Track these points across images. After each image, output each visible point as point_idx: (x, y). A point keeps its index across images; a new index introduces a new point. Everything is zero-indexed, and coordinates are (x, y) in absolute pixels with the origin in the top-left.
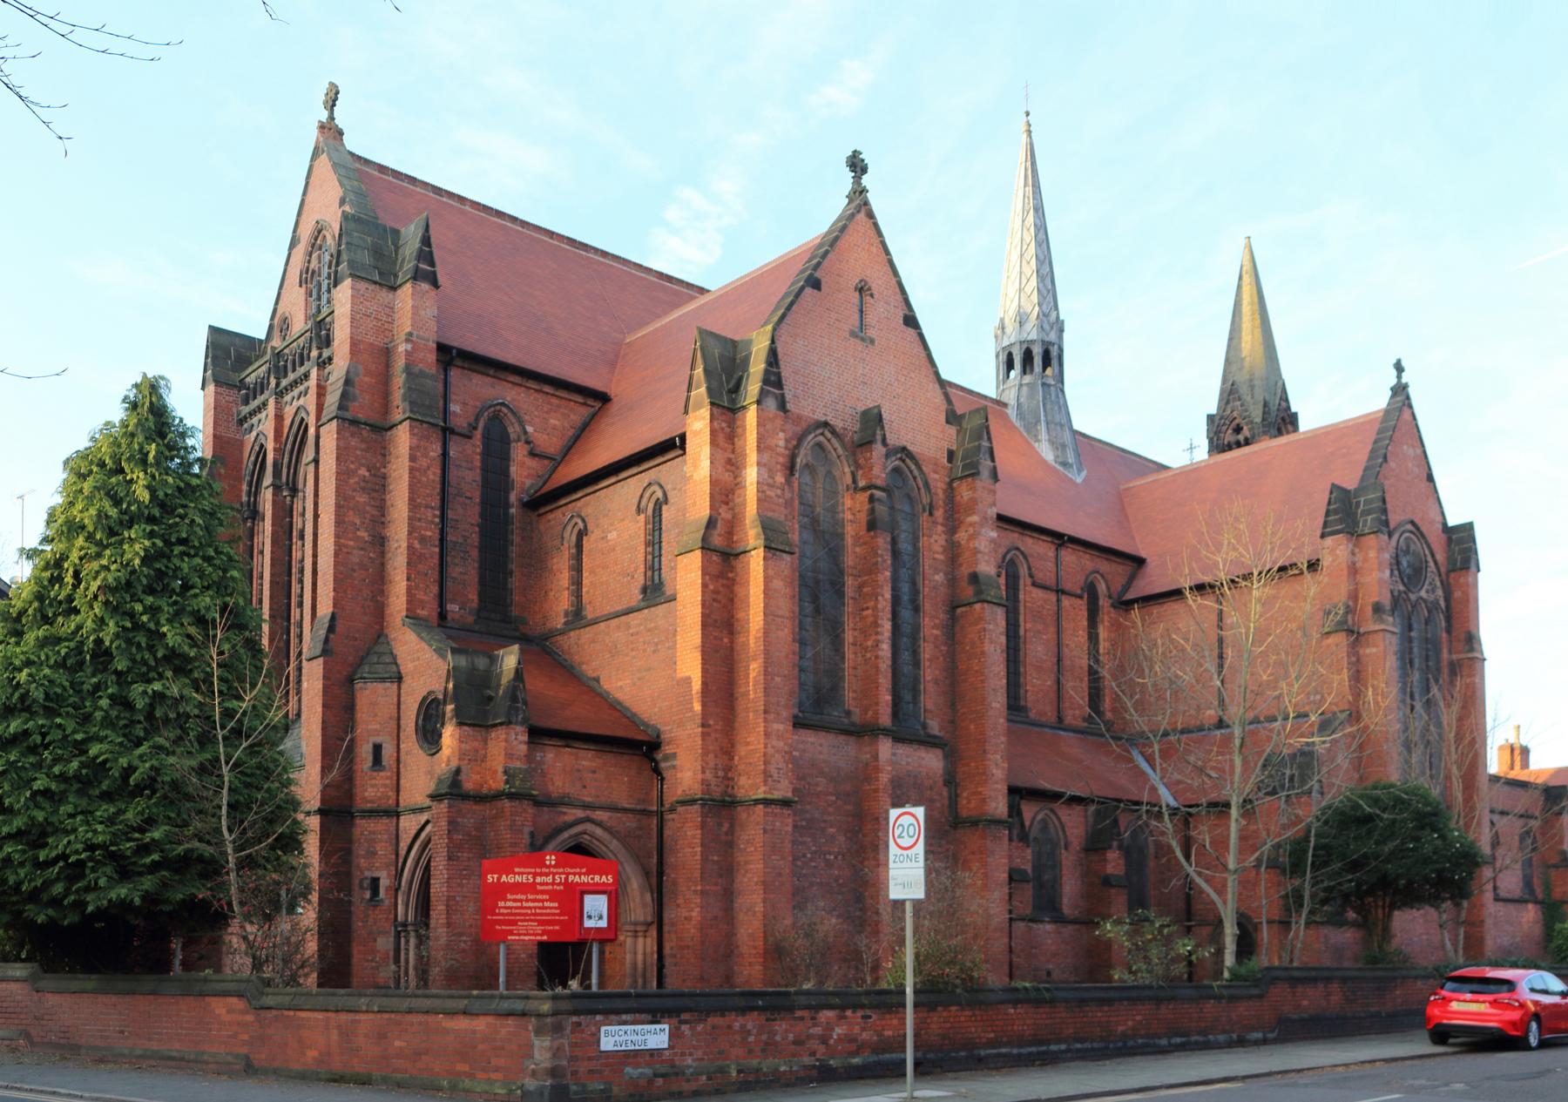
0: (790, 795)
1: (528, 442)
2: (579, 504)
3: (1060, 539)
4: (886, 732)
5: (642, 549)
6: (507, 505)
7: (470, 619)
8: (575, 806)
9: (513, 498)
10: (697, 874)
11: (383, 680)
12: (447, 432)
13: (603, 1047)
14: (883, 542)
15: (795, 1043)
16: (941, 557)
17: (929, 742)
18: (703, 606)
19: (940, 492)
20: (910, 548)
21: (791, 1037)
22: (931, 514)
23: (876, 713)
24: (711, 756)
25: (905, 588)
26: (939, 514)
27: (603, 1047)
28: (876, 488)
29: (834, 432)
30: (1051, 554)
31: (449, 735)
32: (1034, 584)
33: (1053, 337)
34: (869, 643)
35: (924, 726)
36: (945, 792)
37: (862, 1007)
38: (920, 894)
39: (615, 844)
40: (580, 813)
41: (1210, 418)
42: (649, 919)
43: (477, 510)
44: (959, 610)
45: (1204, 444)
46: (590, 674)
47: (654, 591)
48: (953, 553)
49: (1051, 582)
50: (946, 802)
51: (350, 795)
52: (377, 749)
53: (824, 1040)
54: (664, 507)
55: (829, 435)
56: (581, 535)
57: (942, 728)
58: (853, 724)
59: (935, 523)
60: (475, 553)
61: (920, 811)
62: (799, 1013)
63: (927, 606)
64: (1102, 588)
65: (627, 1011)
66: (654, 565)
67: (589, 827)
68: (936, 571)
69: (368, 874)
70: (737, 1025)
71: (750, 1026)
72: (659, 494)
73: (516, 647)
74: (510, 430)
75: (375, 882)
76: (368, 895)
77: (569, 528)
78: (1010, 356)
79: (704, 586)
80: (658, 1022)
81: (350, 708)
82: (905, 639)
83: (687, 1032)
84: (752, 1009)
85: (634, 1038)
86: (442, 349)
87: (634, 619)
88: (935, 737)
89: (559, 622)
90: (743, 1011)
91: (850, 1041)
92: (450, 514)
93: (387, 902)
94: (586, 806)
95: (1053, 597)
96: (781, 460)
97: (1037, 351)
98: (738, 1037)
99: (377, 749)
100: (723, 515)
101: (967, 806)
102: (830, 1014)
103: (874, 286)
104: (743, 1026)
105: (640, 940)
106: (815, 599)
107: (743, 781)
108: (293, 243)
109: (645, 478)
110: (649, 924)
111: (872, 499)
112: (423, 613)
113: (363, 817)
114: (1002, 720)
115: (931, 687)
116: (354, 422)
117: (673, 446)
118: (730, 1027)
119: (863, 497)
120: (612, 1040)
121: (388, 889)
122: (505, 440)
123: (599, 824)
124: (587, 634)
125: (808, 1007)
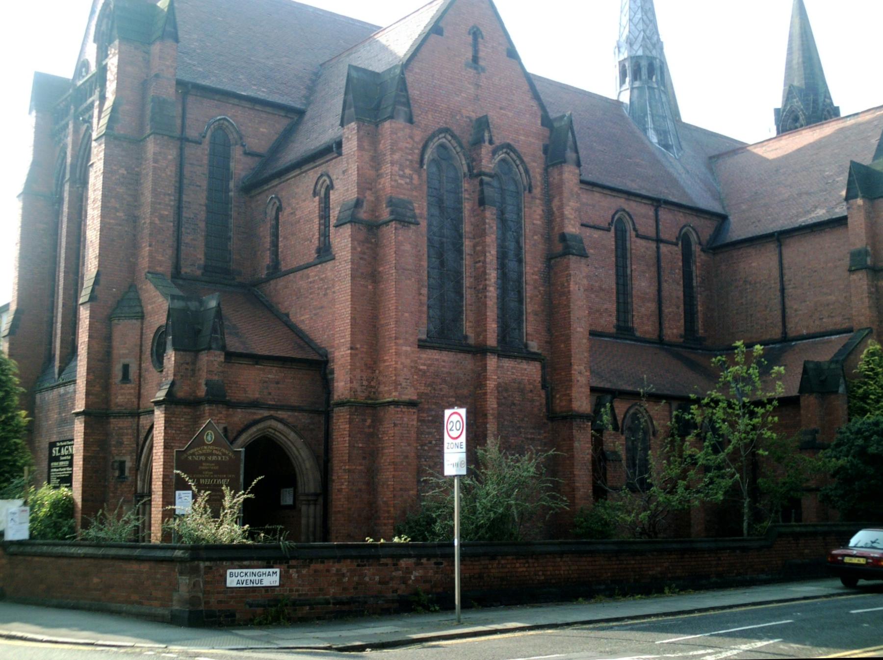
0: (415, 397)
1: (243, 146)
2: (277, 189)
3: (657, 203)
4: (493, 351)
5: (317, 221)
6: (228, 190)
7: (199, 273)
8: (262, 408)
9: (232, 185)
10: (346, 458)
11: (131, 318)
12: (183, 140)
13: (229, 585)
14: (490, 214)
15: (380, 583)
16: (539, 222)
17: (531, 357)
18: (352, 262)
19: (539, 178)
20: (515, 217)
21: (377, 578)
22: (530, 191)
23: (485, 337)
24: (358, 371)
25: (511, 245)
26: (537, 191)
27: (229, 585)
28: (485, 174)
29: (453, 136)
30: (651, 213)
31: (170, 357)
32: (637, 236)
33: (654, 53)
34: (481, 287)
35: (526, 346)
36: (543, 394)
37: (435, 556)
38: (463, 472)
39: (292, 435)
40: (266, 413)
41: (777, 111)
42: (318, 491)
43: (204, 194)
44: (553, 261)
45: (774, 128)
46: (283, 311)
47: (325, 252)
48: (551, 218)
49: (651, 232)
50: (544, 401)
51: (107, 401)
52: (126, 368)
53: (404, 580)
54: (331, 192)
55: (450, 138)
56: (279, 209)
57: (540, 347)
58: (469, 346)
59: (533, 198)
60: (202, 225)
61: (463, 412)
62: (383, 561)
63: (528, 258)
64: (694, 237)
65: (246, 559)
66: (325, 235)
67: (273, 423)
68: (535, 233)
69: (117, 458)
70: (334, 570)
71: (344, 570)
72: (328, 182)
73: (217, 293)
74: (231, 137)
75: (122, 464)
76: (117, 473)
77: (270, 206)
78: (624, 66)
79: (353, 248)
80: (272, 567)
81: (109, 338)
82: (511, 285)
83: (295, 575)
84: (345, 557)
85: (253, 578)
86: (180, 83)
87: (312, 272)
88: (535, 353)
89: (263, 274)
90: (339, 559)
91: (426, 582)
92: (185, 198)
93: (130, 479)
94: (270, 407)
95: (653, 245)
96: (172, 198)
97: (644, 63)
98: (335, 579)
99: (126, 368)
100: (368, 198)
101: (560, 404)
102: (411, 561)
103: (484, 34)
104: (338, 570)
105: (312, 507)
106: (440, 256)
107: (383, 388)
108: (93, 12)
109: (320, 170)
110: (316, 495)
111: (481, 183)
112: (159, 269)
113: (115, 417)
114: (585, 341)
115: (531, 318)
116: (116, 138)
117: (334, 149)
118: (328, 571)
119: (476, 182)
120: (235, 579)
121: (130, 469)
122: (227, 145)
123: (281, 421)
124: (281, 282)
125: (392, 557)
